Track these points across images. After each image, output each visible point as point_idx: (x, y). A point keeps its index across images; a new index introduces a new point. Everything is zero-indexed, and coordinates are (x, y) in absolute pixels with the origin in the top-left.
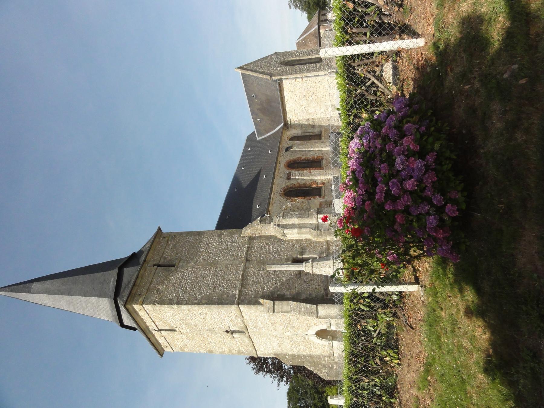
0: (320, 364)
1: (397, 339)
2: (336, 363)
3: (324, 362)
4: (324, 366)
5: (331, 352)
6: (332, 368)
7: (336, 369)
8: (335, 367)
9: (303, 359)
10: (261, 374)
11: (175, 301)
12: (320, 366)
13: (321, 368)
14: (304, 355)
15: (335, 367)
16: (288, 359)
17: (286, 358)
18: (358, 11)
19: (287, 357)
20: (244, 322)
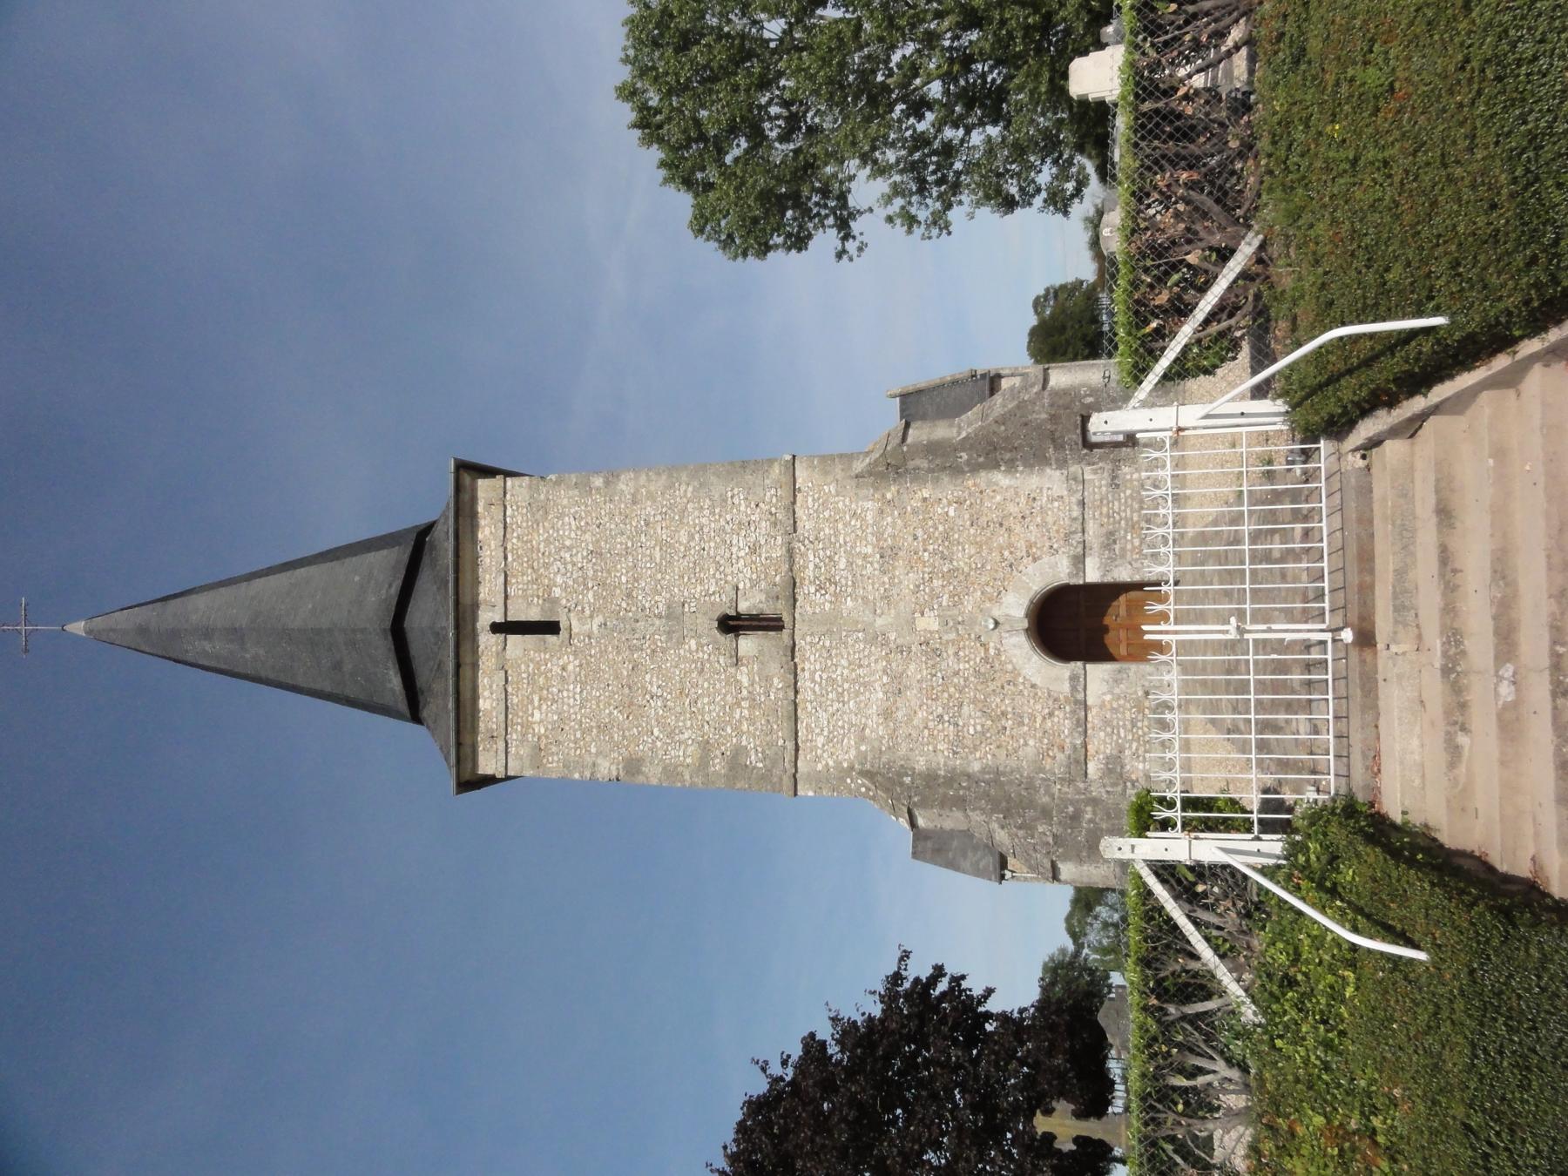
0: (1031, 804)
1: (1515, 705)
2: (1095, 802)
3: (1046, 799)
4: (1046, 814)
5: (781, 737)
6: (1076, 817)
7: (1090, 821)
8: (1088, 816)
9: (968, 788)
10: (701, 239)
11: (1222, 950)
12: (1030, 813)
13: (1035, 819)
14: (969, 776)
15: (1088, 816)
16: (909, 788)
17: (902, 784)
18: (1164, 132)
19: (907, 780)
20: (790, 554)
